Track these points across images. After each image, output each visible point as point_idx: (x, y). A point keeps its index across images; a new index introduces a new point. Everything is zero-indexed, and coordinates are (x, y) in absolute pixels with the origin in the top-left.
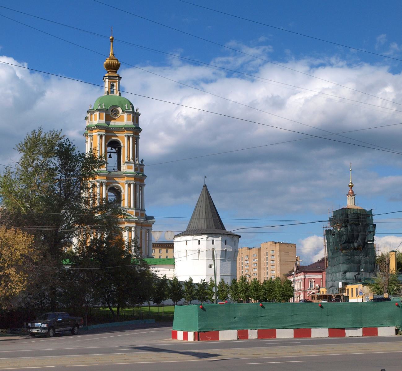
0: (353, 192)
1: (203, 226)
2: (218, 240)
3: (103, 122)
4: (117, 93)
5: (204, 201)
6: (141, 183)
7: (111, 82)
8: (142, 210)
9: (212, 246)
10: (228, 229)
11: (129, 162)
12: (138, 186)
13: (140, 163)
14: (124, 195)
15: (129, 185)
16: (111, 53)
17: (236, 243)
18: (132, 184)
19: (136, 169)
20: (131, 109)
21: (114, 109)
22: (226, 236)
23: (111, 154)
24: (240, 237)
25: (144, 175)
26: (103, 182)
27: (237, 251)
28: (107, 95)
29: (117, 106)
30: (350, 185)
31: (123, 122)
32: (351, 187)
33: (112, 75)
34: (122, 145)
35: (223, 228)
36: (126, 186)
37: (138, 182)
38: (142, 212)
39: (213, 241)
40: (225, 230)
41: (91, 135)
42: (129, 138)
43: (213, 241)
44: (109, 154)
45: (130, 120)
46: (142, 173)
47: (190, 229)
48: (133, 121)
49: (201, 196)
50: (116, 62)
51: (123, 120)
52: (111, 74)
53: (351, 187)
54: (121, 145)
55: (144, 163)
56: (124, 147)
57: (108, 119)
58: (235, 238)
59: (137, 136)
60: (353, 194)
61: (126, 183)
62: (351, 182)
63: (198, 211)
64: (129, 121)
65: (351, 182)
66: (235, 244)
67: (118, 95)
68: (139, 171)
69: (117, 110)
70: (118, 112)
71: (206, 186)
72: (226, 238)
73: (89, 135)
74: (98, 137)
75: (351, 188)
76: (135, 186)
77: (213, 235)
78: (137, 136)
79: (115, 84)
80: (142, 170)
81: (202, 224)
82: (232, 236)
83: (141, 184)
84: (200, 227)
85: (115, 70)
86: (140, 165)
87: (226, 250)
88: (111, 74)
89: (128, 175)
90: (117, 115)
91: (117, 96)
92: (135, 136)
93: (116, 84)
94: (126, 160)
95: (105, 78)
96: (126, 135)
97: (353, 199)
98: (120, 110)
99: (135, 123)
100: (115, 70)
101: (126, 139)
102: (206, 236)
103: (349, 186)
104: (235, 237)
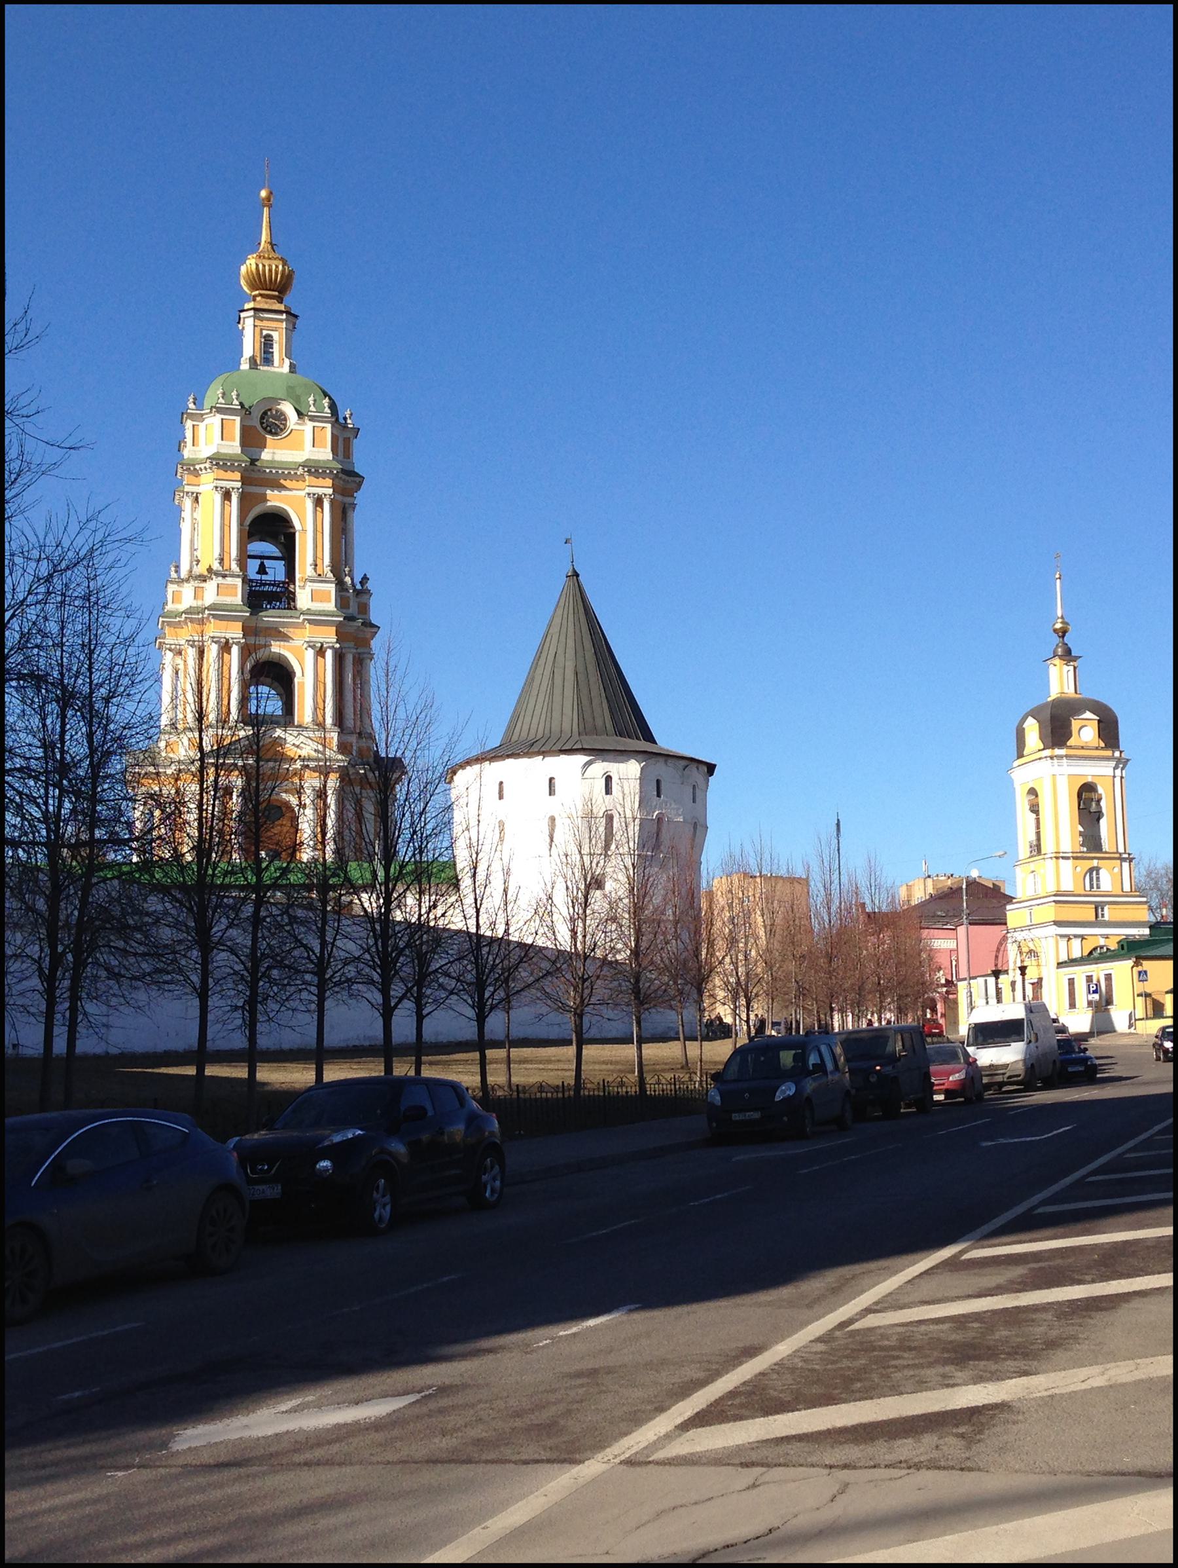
0: (1068, 652)
1: (566, 726)
2: (629, 771)
3: (233, 447)
4: (281, 366)
5: (571, 629)
6: (359, 651)
7: (261, 330)
8: (366, 734)
9: (602, 803)
10: (666, 741)
11: (320, 578)
12: (349, 659)
13: (359, 587)
14: (302, 685)
15: (320, 652)
16: (265, 237)
17: (698, 792)
18: (329, 647)
19: (342, 602)
20: (327, 410)
21: (270, 410)
22: (662, 760)
23: (266, 562)
24: (711, 768)
25: (368, 624)
26: (231, 641)
27: (702, 826)
28: (250, 368)
29: (276, 401)
30: (1058, 626)
31: (301, 452)
32: (1063, 633)
33: (266, 307)
34: (297, 525)
35: (649, 737)
36: (310, 653)
37: (352, 644)
38: (363, 743)
39: (608, 779)
40: (654, 742)
41: (193, 493)
42: (318, 502)
43: (608, 779)
44: (258, 562)
45: (326, 447)
46: (363, 616)
47: (515, 738)
48: (334, 449)
49: (559, 612)
50: (280, 267)
51: (299, 446)
52: (261, 303)
53: (1063, 633)
54: (293, 527)
55: (369, 585)
56: (304, 531)
57: (252, 439)
58: (697, 775)
59: (348, 500)
60: (1068, 655)
61: (310, 646)
62: (1059, 614)
63: (551, 658)
64: (322, 450)
65: (1062, 617)
66: (697, 796)
67: (286, 369)
68: (353, 609)
69: (283, 414)
70: (282, 417)
71: (576, 575)
72: (661, 769)
73: (188, 493)
74: (218, 497)
75: (1063, 637)
76: (339, 658)
77: (611, 756)
78: (348, 500)
79: (275, 335)
80: (364, 609)
81: (567, 720)
82: (683, 763)
83: (359, 654)
84: (556, 728)
85: (276, 293)
86: (358, 593)
87: (659, 819)
88: (261, 303)
89: (317, 619)
90: (282, 430)
91: (282, 374)
92: (339, 497)
93: (280, 335)
94: (310, 572)
95: (243, 315)
96: (309, 494)
97: (1071, 673)
98: (288, 408)
99: (341, 457)
100: (276, 293)
101: (309, 504)
102: (582, 759)
103: (1055, 631)
104: (694, 766)
